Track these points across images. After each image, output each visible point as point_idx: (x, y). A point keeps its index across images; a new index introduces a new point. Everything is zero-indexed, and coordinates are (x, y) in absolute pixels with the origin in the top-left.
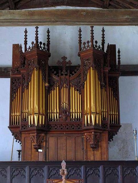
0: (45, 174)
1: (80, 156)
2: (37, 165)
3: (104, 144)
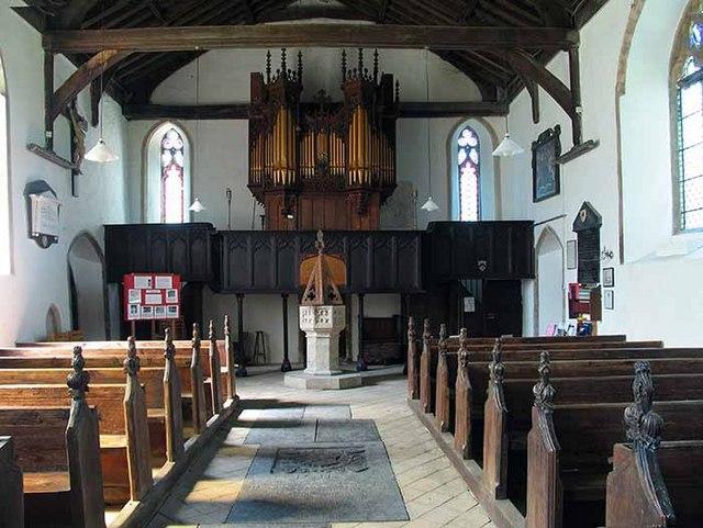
0: (297, 246)
1: (341, 226)
2: (285, 236)
3: (374, 210)
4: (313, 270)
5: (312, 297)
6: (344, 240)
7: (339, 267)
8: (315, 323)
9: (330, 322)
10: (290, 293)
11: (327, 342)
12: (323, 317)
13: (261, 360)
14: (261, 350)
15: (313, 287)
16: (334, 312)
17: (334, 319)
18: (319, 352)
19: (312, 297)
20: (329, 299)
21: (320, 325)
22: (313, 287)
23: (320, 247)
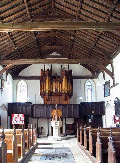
4: (55, 113)
5: (54, 119)
6: (62, 106)
7: (60, 112)
8: (56, 125)
9: (59, 125)
10: (49, 118)
11: (58, 130)
12: (57, 124)
13: (42, 134)
14: (42, 132)
15: (54, 117)
16: (59, 123)
17: (59, 124)
18: (56, 131)
19: (54, 119)
20: (58, 119)
21: (56, 126)
22: (54, 117)
23: (56, 108)
